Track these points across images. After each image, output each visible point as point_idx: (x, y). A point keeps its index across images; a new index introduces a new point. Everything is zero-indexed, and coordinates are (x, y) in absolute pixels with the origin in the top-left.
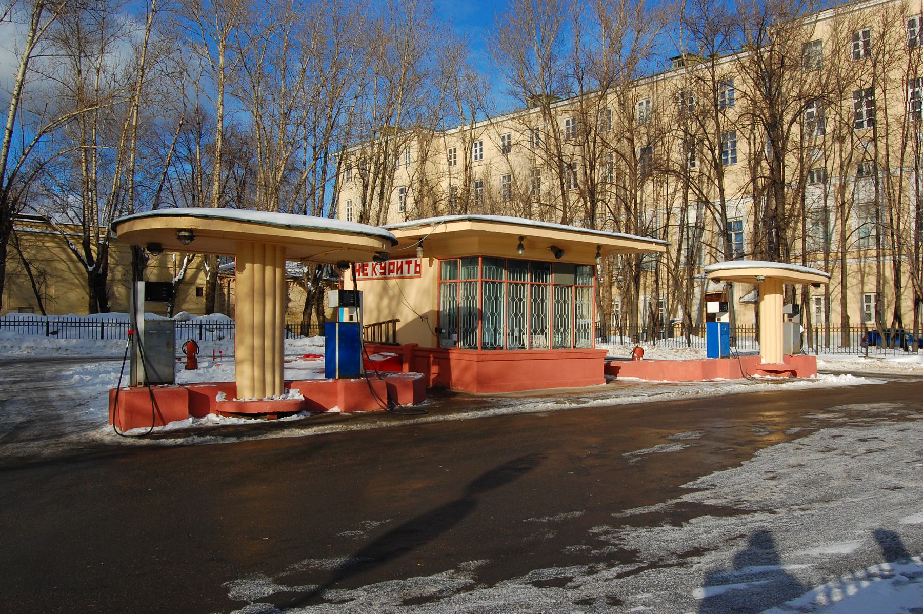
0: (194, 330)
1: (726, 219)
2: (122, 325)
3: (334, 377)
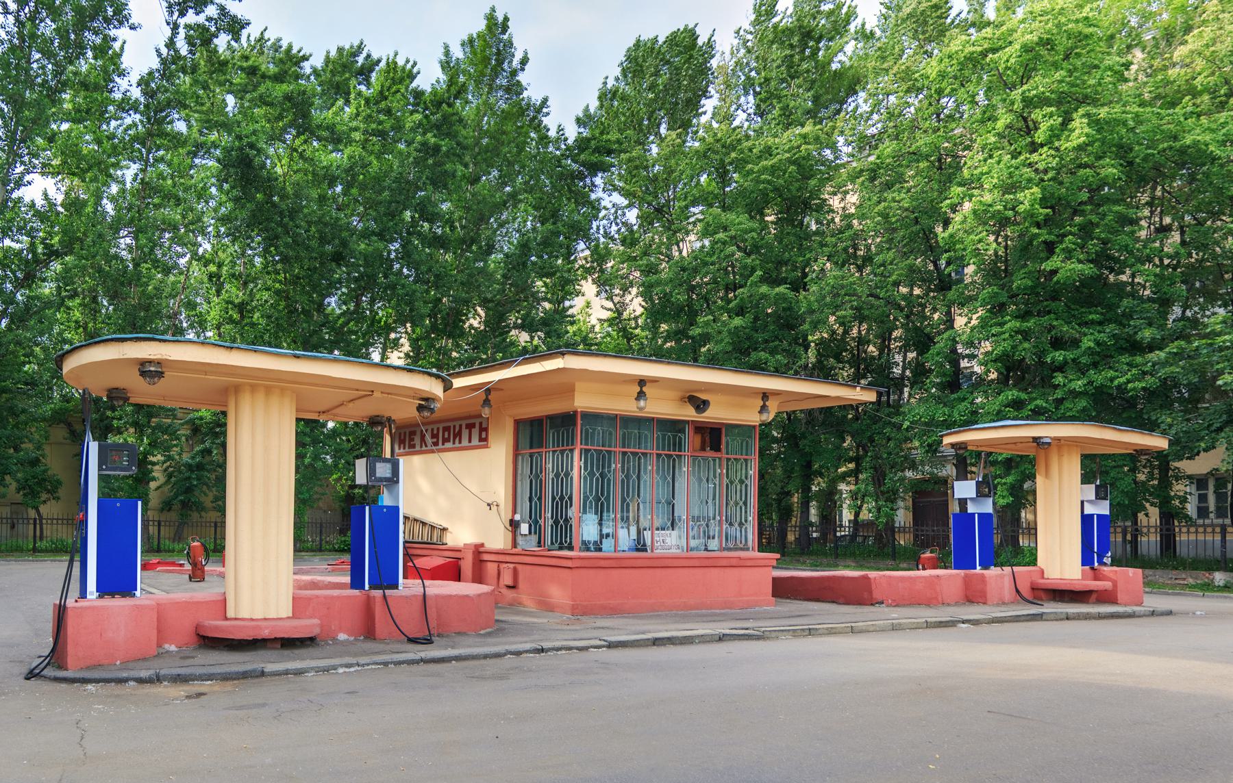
0: (208, 529)
1: (288, 618)
2: (55, 522)
3: (363, 587)
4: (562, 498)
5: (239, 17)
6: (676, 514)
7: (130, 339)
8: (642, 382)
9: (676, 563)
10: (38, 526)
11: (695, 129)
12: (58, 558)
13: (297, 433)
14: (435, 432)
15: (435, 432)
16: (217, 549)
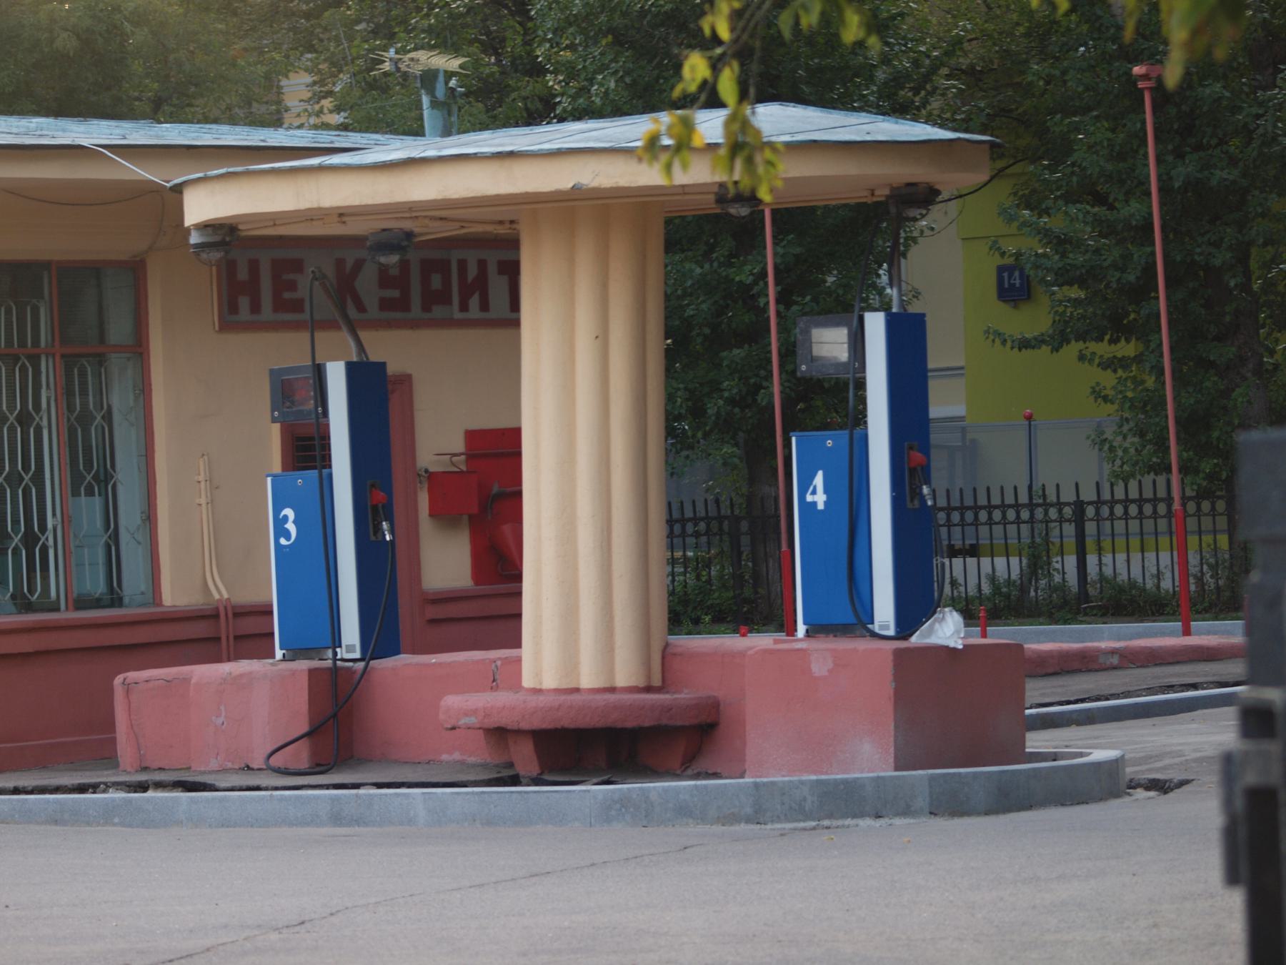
7: (52, 319)
8: (77, 565)
11: (1126, 428)
12: (489, 228)
13: (330, 467)
14: (243, 274)
15: (243, 274)
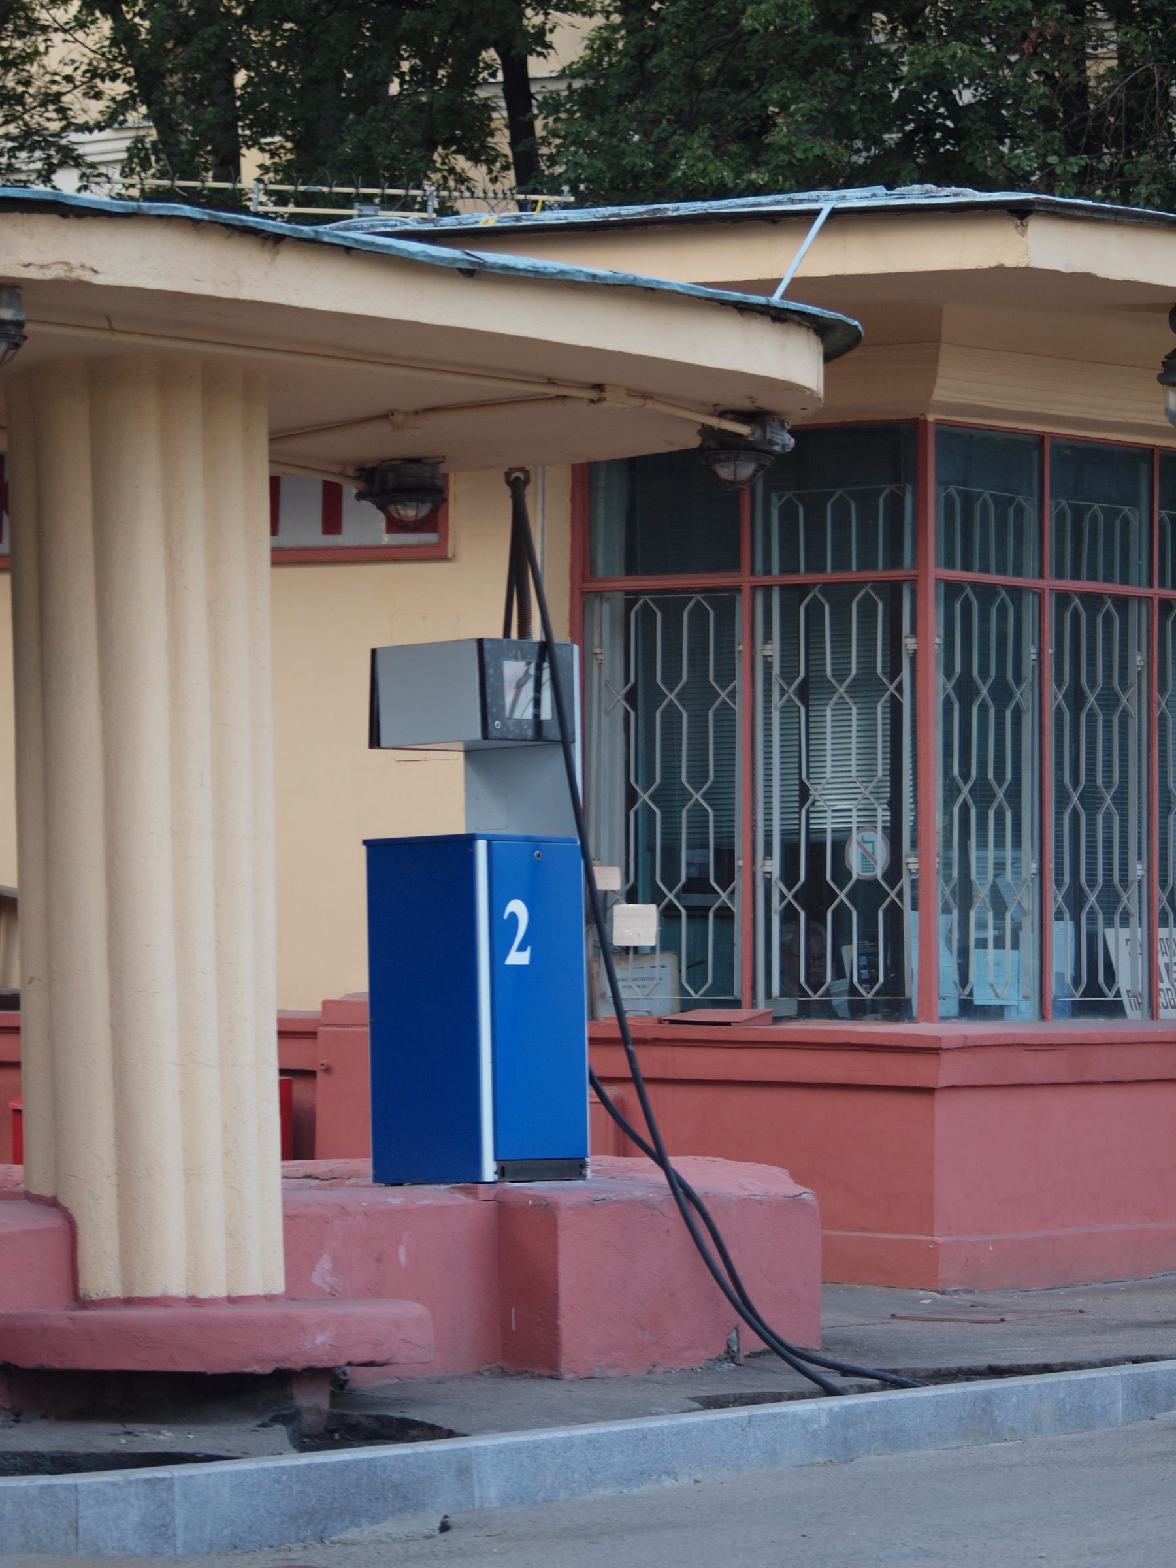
4: (983, 794)
5: (574, 15)
6: (548, 75)
9: (1046, 1048)
10: (725, 746)
16: (504, 1373)
